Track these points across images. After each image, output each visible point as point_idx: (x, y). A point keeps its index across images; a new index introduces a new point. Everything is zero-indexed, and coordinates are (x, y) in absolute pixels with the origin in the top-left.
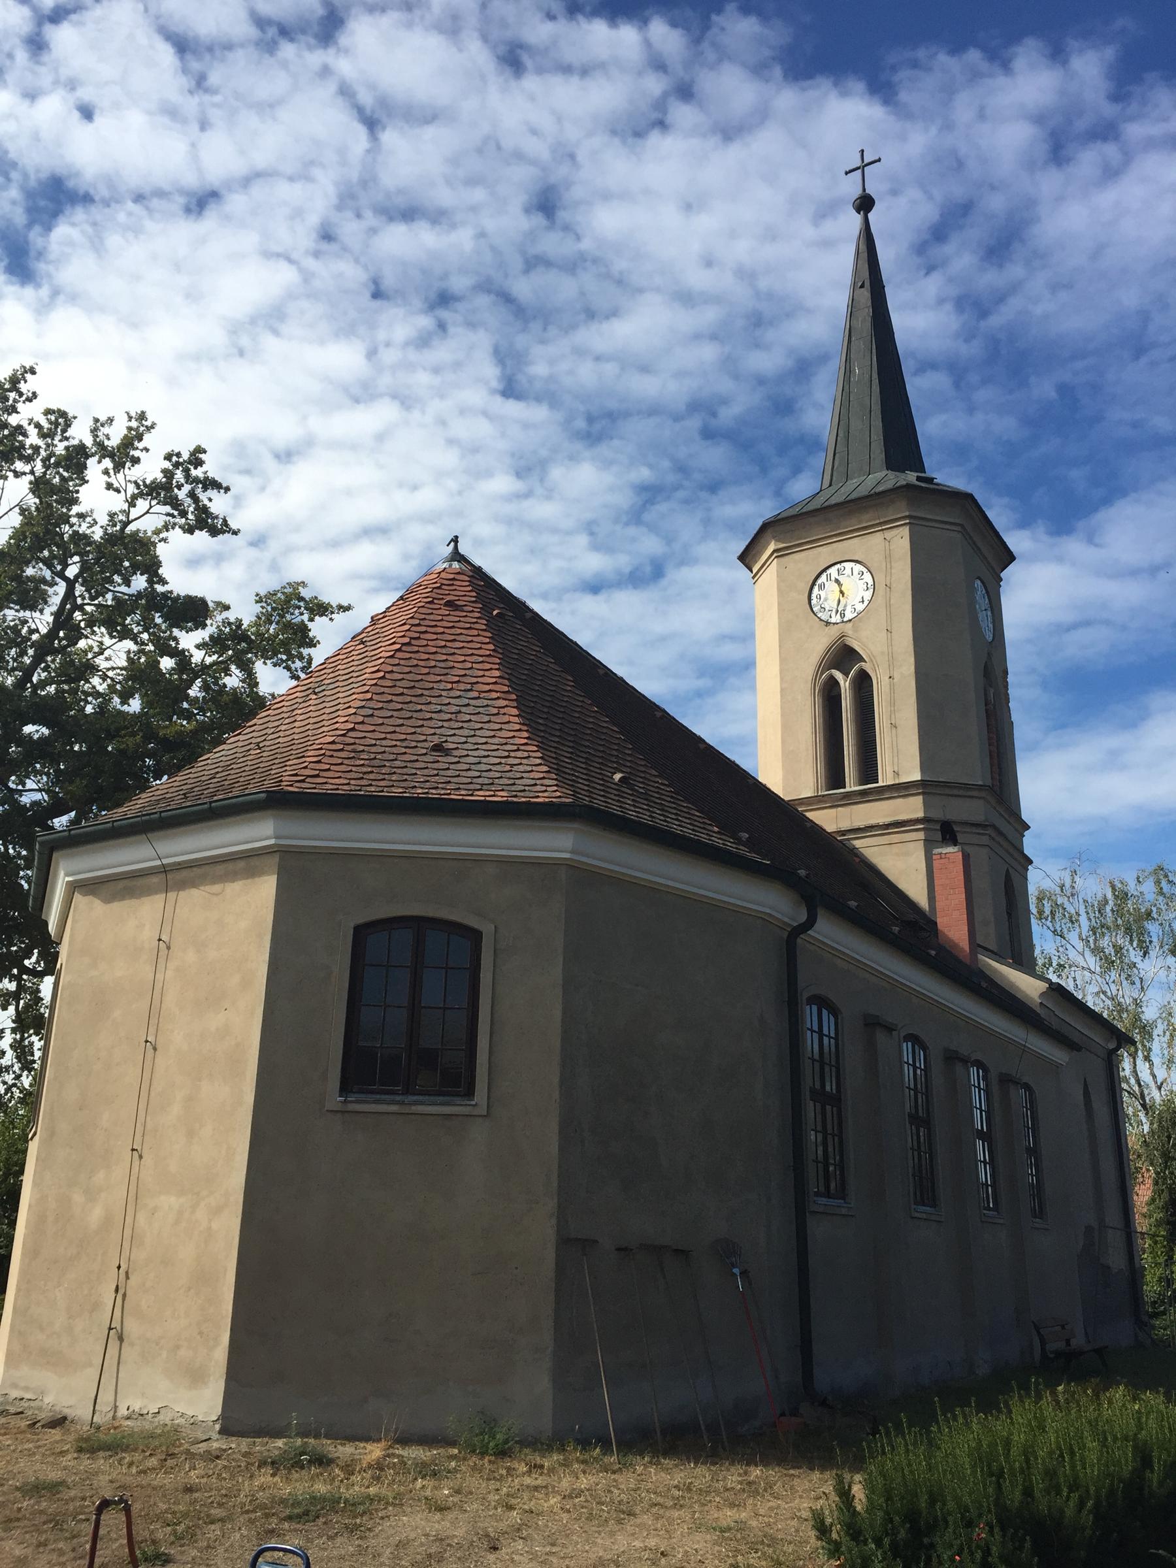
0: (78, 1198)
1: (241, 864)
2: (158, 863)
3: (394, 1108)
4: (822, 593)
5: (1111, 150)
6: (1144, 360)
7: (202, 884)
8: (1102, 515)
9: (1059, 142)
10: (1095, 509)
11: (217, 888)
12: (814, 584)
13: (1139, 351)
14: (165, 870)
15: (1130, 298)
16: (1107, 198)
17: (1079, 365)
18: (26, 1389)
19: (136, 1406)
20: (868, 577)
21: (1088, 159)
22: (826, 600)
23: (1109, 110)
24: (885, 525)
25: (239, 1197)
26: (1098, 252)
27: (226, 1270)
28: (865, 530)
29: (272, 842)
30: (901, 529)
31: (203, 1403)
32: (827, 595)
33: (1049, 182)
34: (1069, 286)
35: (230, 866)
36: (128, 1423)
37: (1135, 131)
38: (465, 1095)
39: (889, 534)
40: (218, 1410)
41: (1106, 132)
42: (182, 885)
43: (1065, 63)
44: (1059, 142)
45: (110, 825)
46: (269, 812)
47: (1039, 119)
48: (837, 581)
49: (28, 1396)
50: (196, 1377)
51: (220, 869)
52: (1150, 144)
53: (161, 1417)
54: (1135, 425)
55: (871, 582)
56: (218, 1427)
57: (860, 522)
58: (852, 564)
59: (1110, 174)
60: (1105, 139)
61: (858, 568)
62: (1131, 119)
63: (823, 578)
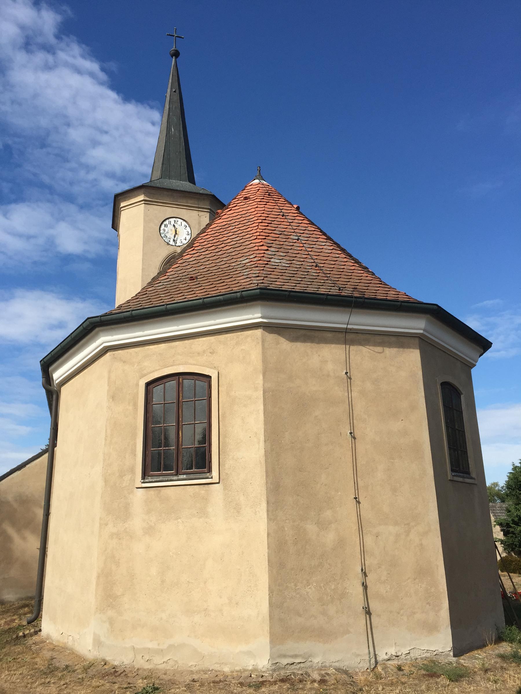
0: (311, 528)
1: (393, 339)
2: (345, 326)
3: (461, 479)
4: (166, 229)
5: (50, 58)
6: (44, 150)
7: (367, 345)
8: (13, 206)
9: (29, 43)
10: (10, 202)
11: (379, 349)
12: (162, 223)
13: (43, 146)
14: (346, 331)
15: (44, 122)
16: (44, 77)
17: (17, 140)
18: (296, 656)
19: (392, 651)
20: (188, 229)
21: (40, 57)
22: (168, 232)
23: (53, 40)
24: (199, 208)
25: (436, 527)
26: (35, 96)
27: (437, 566)
28: (189, 207)
29: (421, 332)
30: (206, 213)
31: (440, 643)
32: (168, 230)
33: (21, 57)
34: (20, 104)
35: (386, 339)
36: (389, 662)
37: (62, 55)
38: (451, 469)
39: (201, 214)
40: (451, 645)
41: (49, 49)
42: (352, 342)
43: (39, 10)
44: (29, 43)
45: (325, 297)
46: (423, 315)
47: (22, 27)
48: (174, 226)
49: (297, 661)
50: (431, 628)
51: (378, 339)
52: (67, 65)
53: (412, 655)
54: (35, 175)
55: (190, 232)
56: (452, 654)
57: (187, 203)
58: (182, 221)
59: (48, 68)
60: (48, 52)
61: (184, 223)
62: (62, 50)
63: (167, 222)
